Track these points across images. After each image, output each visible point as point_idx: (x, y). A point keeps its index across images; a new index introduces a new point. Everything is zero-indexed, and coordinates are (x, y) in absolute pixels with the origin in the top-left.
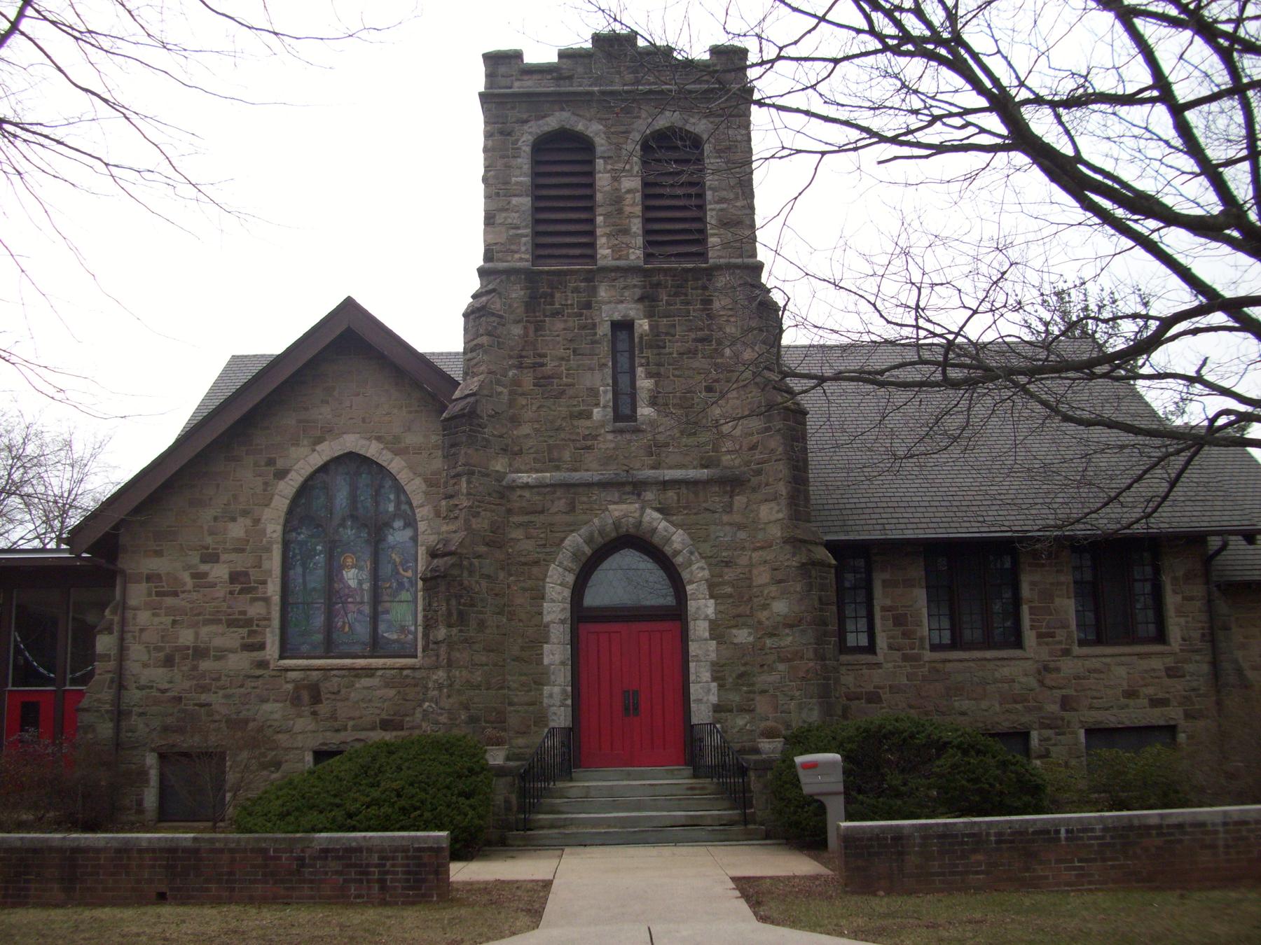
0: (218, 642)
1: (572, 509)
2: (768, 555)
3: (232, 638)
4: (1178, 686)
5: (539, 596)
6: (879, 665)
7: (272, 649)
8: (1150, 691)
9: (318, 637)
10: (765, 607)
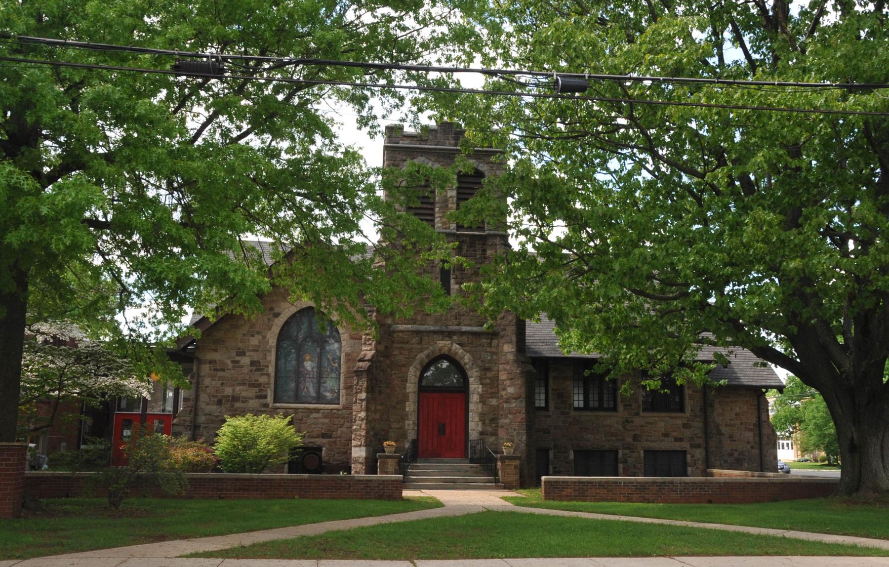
0: (244, 394)
1: (420, 342)
2: (508, 367)
3: (253, 392)
4: (688, 433)
5: (405, 381)
6: (549, 416)
7: (270, 399)
8: (675, 434)
9: (291, 394)
10: (504, 389)
